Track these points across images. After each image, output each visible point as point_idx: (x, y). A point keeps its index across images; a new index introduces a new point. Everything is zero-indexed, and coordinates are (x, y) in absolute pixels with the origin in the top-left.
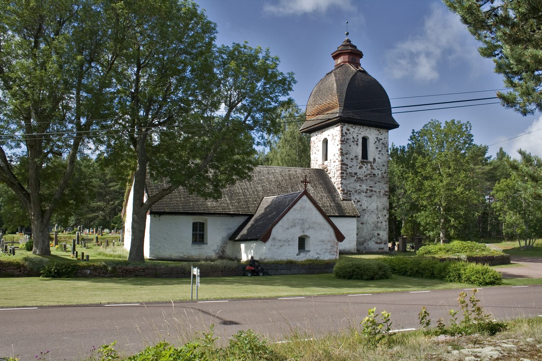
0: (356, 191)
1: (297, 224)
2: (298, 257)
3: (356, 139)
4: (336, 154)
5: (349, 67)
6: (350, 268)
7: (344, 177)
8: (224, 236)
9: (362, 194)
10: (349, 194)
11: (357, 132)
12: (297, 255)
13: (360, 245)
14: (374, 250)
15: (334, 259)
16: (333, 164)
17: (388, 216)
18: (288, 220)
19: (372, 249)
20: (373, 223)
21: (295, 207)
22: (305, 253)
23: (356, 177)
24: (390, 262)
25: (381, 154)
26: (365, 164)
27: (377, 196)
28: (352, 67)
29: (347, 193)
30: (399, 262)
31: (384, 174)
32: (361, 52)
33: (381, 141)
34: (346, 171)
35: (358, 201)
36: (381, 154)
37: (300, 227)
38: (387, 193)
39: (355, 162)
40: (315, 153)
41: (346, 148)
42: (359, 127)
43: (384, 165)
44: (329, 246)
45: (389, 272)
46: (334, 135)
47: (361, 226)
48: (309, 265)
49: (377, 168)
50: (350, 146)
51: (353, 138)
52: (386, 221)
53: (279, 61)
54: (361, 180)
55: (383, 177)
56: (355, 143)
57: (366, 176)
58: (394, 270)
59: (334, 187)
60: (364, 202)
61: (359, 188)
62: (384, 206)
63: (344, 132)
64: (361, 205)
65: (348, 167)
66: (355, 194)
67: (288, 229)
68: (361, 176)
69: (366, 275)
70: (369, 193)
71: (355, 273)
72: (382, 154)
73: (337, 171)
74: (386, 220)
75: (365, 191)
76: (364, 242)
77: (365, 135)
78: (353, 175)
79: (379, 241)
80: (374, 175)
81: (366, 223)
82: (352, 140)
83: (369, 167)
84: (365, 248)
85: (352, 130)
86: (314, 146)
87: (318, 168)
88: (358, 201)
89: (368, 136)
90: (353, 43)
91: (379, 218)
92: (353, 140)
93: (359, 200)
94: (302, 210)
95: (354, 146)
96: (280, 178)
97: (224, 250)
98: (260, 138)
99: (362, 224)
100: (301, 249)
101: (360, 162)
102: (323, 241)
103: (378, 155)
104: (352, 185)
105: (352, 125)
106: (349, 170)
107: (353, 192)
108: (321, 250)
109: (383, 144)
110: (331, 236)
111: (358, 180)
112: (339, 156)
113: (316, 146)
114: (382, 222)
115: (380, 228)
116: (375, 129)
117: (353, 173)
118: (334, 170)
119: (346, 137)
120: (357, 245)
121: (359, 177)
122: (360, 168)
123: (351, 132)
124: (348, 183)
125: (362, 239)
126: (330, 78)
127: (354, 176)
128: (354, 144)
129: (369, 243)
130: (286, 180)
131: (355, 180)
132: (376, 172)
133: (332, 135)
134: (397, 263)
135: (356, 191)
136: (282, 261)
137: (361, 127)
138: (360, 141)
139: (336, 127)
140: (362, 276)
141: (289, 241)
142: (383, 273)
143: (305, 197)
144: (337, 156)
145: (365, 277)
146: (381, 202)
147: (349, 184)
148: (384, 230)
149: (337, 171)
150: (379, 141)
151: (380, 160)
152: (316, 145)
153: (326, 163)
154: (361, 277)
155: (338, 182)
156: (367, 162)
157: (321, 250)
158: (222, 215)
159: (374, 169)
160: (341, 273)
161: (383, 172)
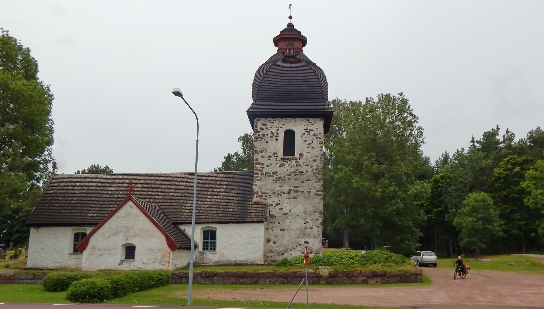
0: (274, 193)
1: (120, 232)
2: (119, 267)
3: (275, 134)
9: (283, 195)
11: (277, 125)
12: (119, 265)
15: (166, 269)
18: (110, 227)
20: (298, 229)
23: (275, 176)
25: (310, 148)
26: (288, 161)
27: (304, 198)
29: (261, 196)
33: (312, 133)
35: (277, 204)
36: (310, 148)
37: (123, 235)
38: (319, 193)
42: (280, 119)
44: (159, 256)
49: (305, 164)
50: (267, 142)
51: (272, 133)
54: (282, 180)
56: (274, 138)
57: (289, 175)
61: (279, 189)
64: (281, 209)
65: (264, 166)
66: (273, 196)
67: (109, 237)
68: (282, 176)
70: (293, 194)
74: (319, 225)
76: (285, 252)
78: (271, 175)
80: (301, 172)
81: (288, 229)
85: (269, 125)
88: (277, 204)
91: (308, 222)
92: (272, 135)
102: (152, 250)
106: (266, 170)
107: (270, 194)
108: (148, 260)
109: (314, 135)
110: (162, 245)
114: (312, 228)
116: (302, 119)
117: (271, 173)
119: (261, 134)
121: (279, 176)
122: (281, 166)
123: (269, 127)
127: (273, 176)
131: (274, 180)
132: (304, 169)
135: (274, 193)
141: (110, 250)
143: (130, 203)
148: (315, 237)
150: (309, 132)
157: (148, 260)
159: (300, 165)
161: (314, 168)
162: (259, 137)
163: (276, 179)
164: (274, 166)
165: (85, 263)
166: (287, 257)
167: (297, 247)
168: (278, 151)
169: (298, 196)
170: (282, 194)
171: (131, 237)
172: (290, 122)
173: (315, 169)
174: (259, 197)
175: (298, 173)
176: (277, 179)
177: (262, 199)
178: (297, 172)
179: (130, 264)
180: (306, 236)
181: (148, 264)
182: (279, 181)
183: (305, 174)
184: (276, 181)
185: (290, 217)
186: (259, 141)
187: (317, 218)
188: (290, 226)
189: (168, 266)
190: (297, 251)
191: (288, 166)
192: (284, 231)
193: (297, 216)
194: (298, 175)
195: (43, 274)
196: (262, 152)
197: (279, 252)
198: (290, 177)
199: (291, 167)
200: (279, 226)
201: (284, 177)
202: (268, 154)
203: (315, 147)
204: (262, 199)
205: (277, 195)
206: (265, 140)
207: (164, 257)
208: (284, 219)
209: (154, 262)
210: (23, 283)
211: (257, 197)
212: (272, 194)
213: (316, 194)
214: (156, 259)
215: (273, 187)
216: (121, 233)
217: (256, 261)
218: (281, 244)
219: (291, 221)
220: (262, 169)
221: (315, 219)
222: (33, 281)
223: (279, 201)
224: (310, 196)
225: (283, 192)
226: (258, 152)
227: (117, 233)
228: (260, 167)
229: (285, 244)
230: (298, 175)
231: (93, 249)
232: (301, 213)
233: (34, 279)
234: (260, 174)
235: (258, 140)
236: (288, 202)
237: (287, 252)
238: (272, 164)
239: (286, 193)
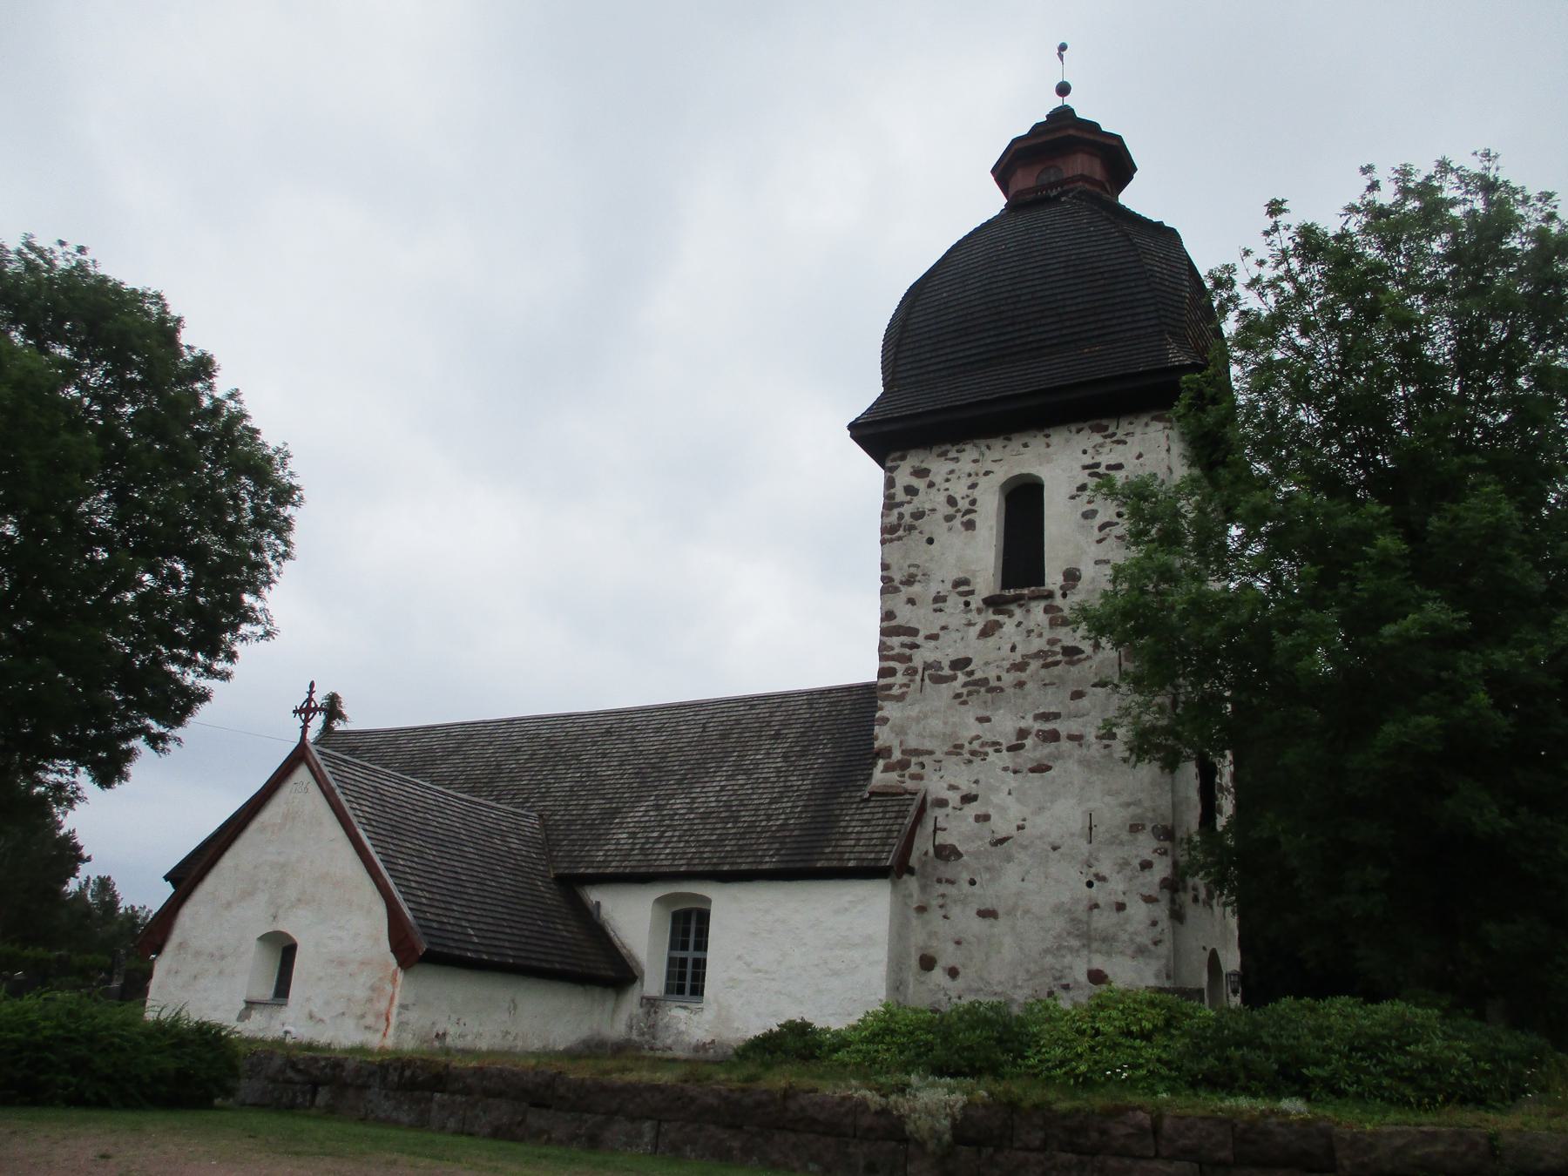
7: (895, 691)
20: (1058, 909)
26: (1013, 607)
27: (1086, 763)
35: (968, 799)
51: (952, 501)
56: (957, 522)
57: (1020, 667)
60: (1000, 798)
61: (975, 729)
68: (992, 674)
70: (1034, 750)
78: (947, 672)
85: (939, 468)
88: (968, 799)
91: (1102, 879)
92: (951, 510)
93: (974, 789)
99: (987, 914)
104: (936, 724)
107: (939, 755)
111: (970, 694)
114: (1121, 907)
115: (1107, 939)
117: (946, 664)
122: (988, 631)
127: (954, 678)
131: (958, 696)
146: (1110, 793)
148: (1141, 951)
163: (965, 691)
170: (990, 750)
172: (1025, 445)
175: (1059, 657)
177: (903, 776)
178: (1054, 653)
180: (1095, 945)
183: (1089, 658)
185: (1021, 856)
187: (1147, 854)
188: (1019, 894)
189: (385, 1035)
193: (1055, 849)
194: (1056, 663)
199: (1029, 632)
200: (973, 895)
201: (999, 679)
202: (934, 588)
204: (903, 776)
205: (967, 756)
209: (343, 1014)
212: (948, 753)
215: (954, 724)
218: (982, 979)
219: (1028, 872)
220: (907, 651)
221: (1136, 863)
223: (976, 782)
226: (896, 583)
228: (903, 645)
229: (1000, 983)
232: (1072, 835)
234: (899, 675)
236: (1013, 784)
238: (951, 627)
239: (1004, 747)
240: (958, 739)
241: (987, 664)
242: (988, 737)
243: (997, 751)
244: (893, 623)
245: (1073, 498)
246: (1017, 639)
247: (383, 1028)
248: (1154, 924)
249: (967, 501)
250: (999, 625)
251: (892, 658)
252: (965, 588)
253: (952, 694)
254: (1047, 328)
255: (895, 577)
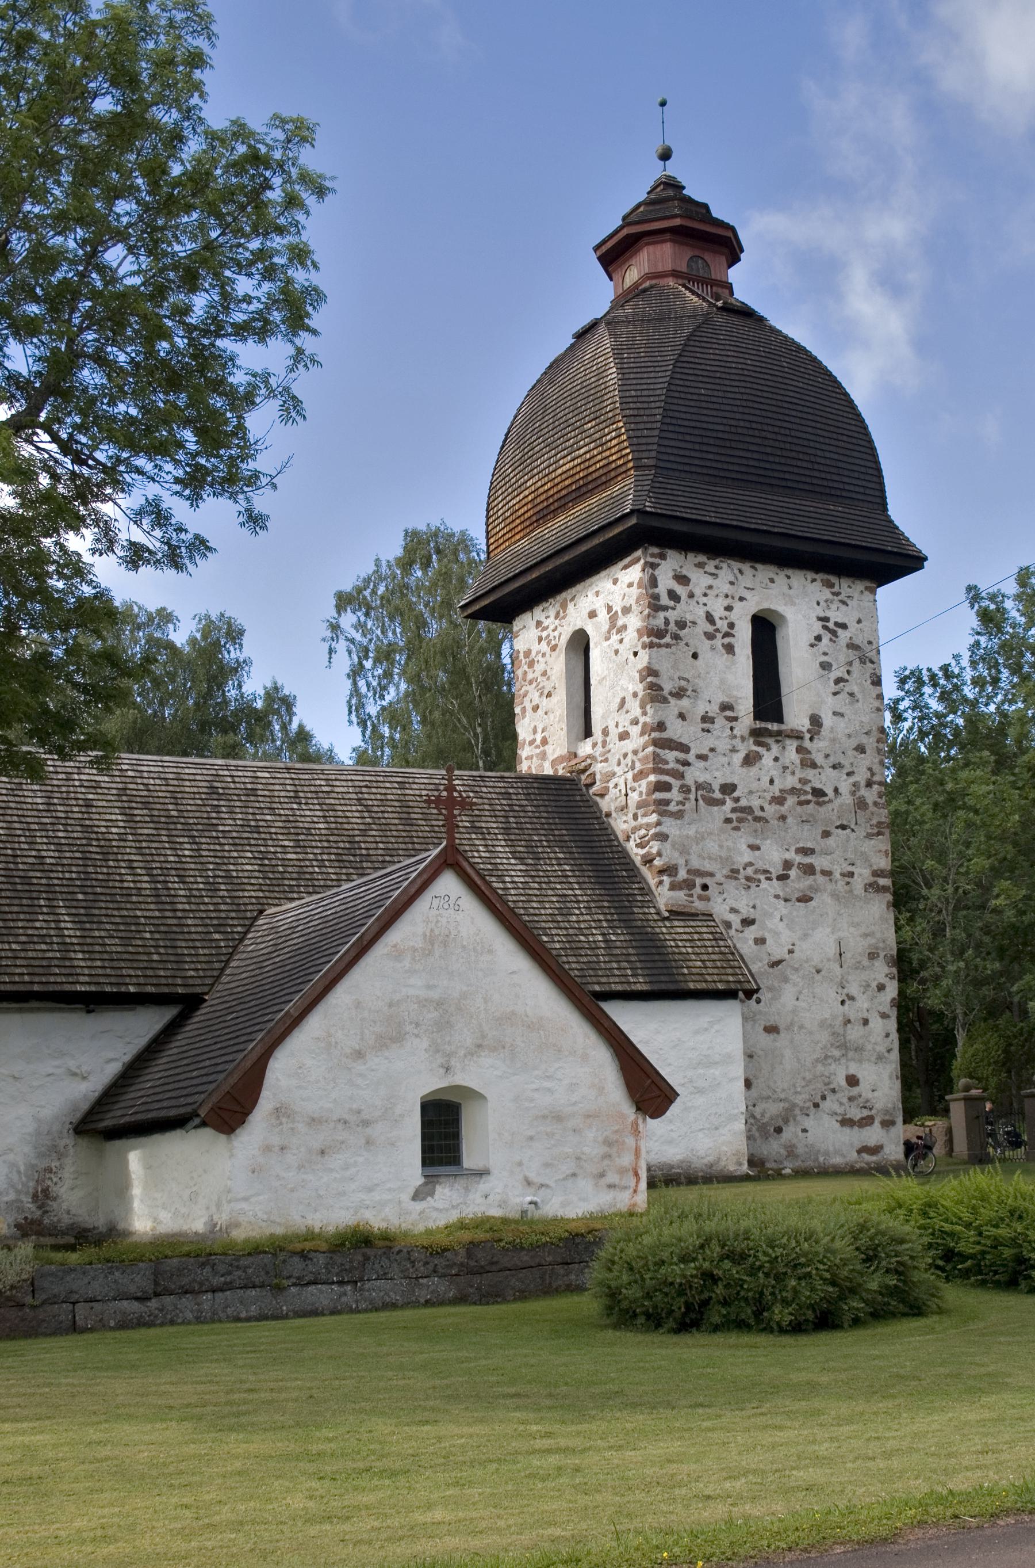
1: (409, 1028)
2: (419, 1206)
4: (629, 699)
5: (678, 295)
6: (684, 1259)
7: (673, 807)
8: (47, 1113)
9: (764, 884)
10: (698, 890)
11: (726, 588)
12: (417, 1196)
13: (766, 1136)
14: (837, 1160)
16: (618, 747)
17: (892, 990)
18: (358, 1005)
19: (827, 1153)
20: (823, 1024)
21: (395, 936)
22: (461, 1182)
23: (729, 804)
24: (925, 1214)
25: (843, 696)
26: (770, 741)
27: (835, 896)
28: (693, 293)
29: (689, 885)
30: (974, 1211)
31: (863, 792)
32: (733, 229)
34: (681, 776)
35: (747, 922)
36: (843, 696)
37: (425, 1044)
38: (883, 882)
39: (720, 737)
40: (536, 708)
41: (675, 666)
42: (736, 565)
43: (861, 749)
44: (591, 1144)
45: (923, 1276)
46: (618, 608)
47: (765, 1040)
48: (472, 1247)
49: (832, 760)
50: (695, 656)
51: (710, 618)
52: (884, 1016)
53: (307, 213)
54: (758, 819)
55: (861, 804)
56: (719, 642)
57: (779, 800)
58: (949, 1255)
59: (624, 855)
60: (774, 923)
61: (747, 856)
62: (871, 941)
63: (662, 589)
64: (760, 941)
65: (691, 757)
66: (730, 886)
67: (359, 1055)
68: (755, 803)
69: (786, 1302)
70: (798, 882)
71: (720, 1290)
72: (851, 694)
73: (636, 778)
75: (776, 870)
76: (786, 1121)
77: (765, 605)
78: (717, 795)
79: (856, 1114)
80: (818, 793)
82: (705, 627)
83: (791, 755)
84: (791, 1152)
85: (699, 580)
86: (530, 676)
87: (548, 771)
88: (747, 922)
89: (780, 609)
90: (693, 191)
91: (852, 998)
92: (710, 628)
93: (752, 914)
94: (438, 951)
95: (712, 658)
96: (354, 815)
97: (46, 1191)
98: (146, 522)
99: (771, 1030)
100: (441, 1162)
101: (746, 732)
103: (830, 700)
104: (712, 846)
105: (702, 558)
106: (695, 774)
107: (719, 877)
108: (547, 1165)
109: (852, 646)
110: (601, 1090)
111: (740, 820)
112: (643, 706)
113: (537, 674)
114: (866, 1022)
115: (859, 1049)
116: (810, 575)
117: (716, 787)
118: (622, 778)
120: (749, 1138)
121: (743, 803)
122: (750, 760)
123: (698, 592)
124: (691, 832)
125: (772, 1109)
126: (592, 347)
127: (723, 803)
128: (713, 648)
129: (809, 1123)
130: (384, 828)
131: (728, 821)
132: (825, 779)
133: (610, 608)
134: (966, 1216)
136: (310, 1236)
137: (746, 567)
138: (744, 634)
139: (625, 567)
140: (761, 1308)
141: (366, 1123)
142: (892, 1281)
143: (448, 884)
144: (635, 708)
145: (780, 1314)
146: (853, 925)
147: (699, 838)
148: (880, 1058)
149: (636, 778)
150: (834, 633)
151: (841, 724)
152: (539, 668)
153: (585, 748)
154: (758, 1314)
155: (643, 832)
156: (779, 733)
157: (547, 1165)
158: (35, 1004)
159: (814, 765)
160: (633, 1292)
161: (861, 777)
162: (667, 631)
163: (734, 816)
164: (725, 760)
165: (246, 1199)
166: (794, 1141)
167: (824, 1098)
168: (737, 698)
169: (817, 890)
170: (762, 877)
171: (462, 1052)
172: (772, 581)
173: (863, 783)
174: (681, 889)
175: (809, 797)
176: (739, 814)
177: (691, 896)
178: (806, 793)
179: (467, 1189)
180: (851, 1054)
181: (547, 1186)
182: (746, 824)
183: (830, 801)
184: (735, 824)
185: (794, 977)
186: (668, 646)
187: (883, 980)
188: (794, 1011)
189: (635, 1191)
190: (826, 1118)
191: (771, 763)
192: (778, 1033)
193: (818, 972)
194: (808, 802)
195: (203, 1265)
196: (679, 694)
197: (765, 1120)
198: (784, 809)
199: (785, 768)
200: (760, 1012)
201: (762, 809)
202: (701, 708)
203: (859, 696)
204: (691, 896)
205: (743, 881)
206: (687, 644)
207: (613, 1151)
208: (776, 984)
209: (574, 1175)
210: (101, 1326)
211: (673, 887)
212: (727, 877)
213: (871, 885)
214: (578, 1158)
215: (729, 849)
216: (417, 1036)
217: (723, 1163)
218: (769, 1087)
219: (800, 993)
220: (681, 768)
221: (874, 985)
222: (154, 1304)
223: (754, 907)
224: (851, 891)
225: (766, 872)
226: (666, 693)
227: (399, 1038)
228: (678, 761)
229: (784, 1090)
230: (808, 802)
231: (284, 1120)
232: (829, 960)
233: (157, 1295)
234: (675, 790)
235: (663, 641)
236: (784, 912)
237: (792, 1122)
238: (718, 750)
239: (774, 876)
240: (733, 863)
241: (751, 792)
242: (760, 865)
243: (769, 879)
244: (664, 735)
245: (812, 646)
246: (774, 773)
247: (633, 1184)
248: (887, 1035)
249: (725, 622)
250: (758, 757)
251: (667, 772)
252: (729, 713)
253: (723, 818)
254: (802, 471)
255: (664, 686)
